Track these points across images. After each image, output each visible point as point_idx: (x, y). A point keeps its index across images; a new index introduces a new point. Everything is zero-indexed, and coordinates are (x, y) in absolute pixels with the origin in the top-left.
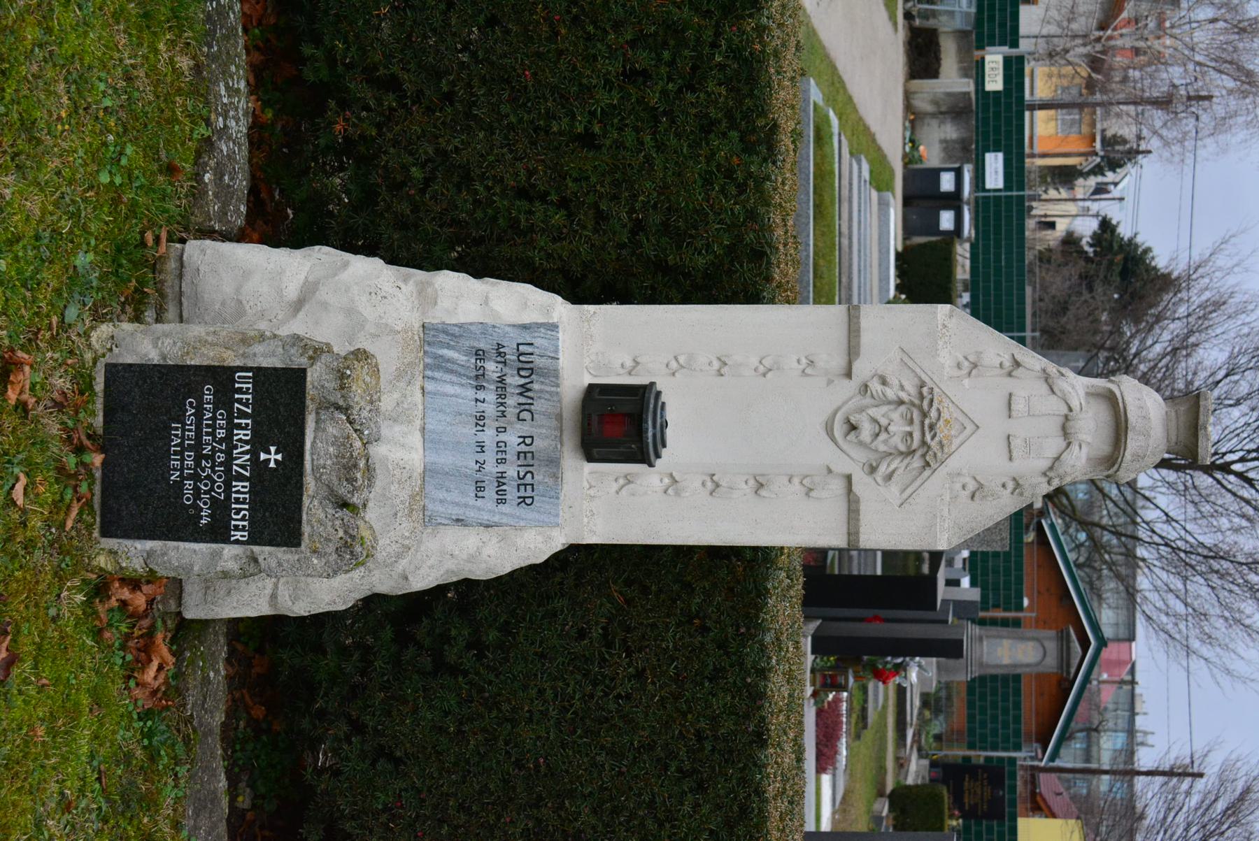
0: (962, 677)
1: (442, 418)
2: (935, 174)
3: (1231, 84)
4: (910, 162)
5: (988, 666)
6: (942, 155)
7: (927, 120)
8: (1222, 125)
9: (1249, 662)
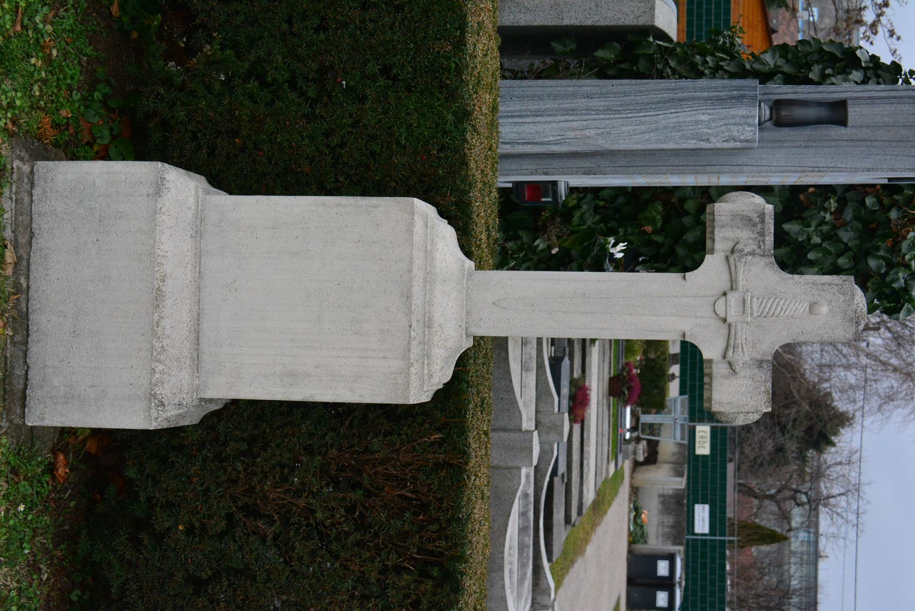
1: (229, 296)
6: (660, 507)
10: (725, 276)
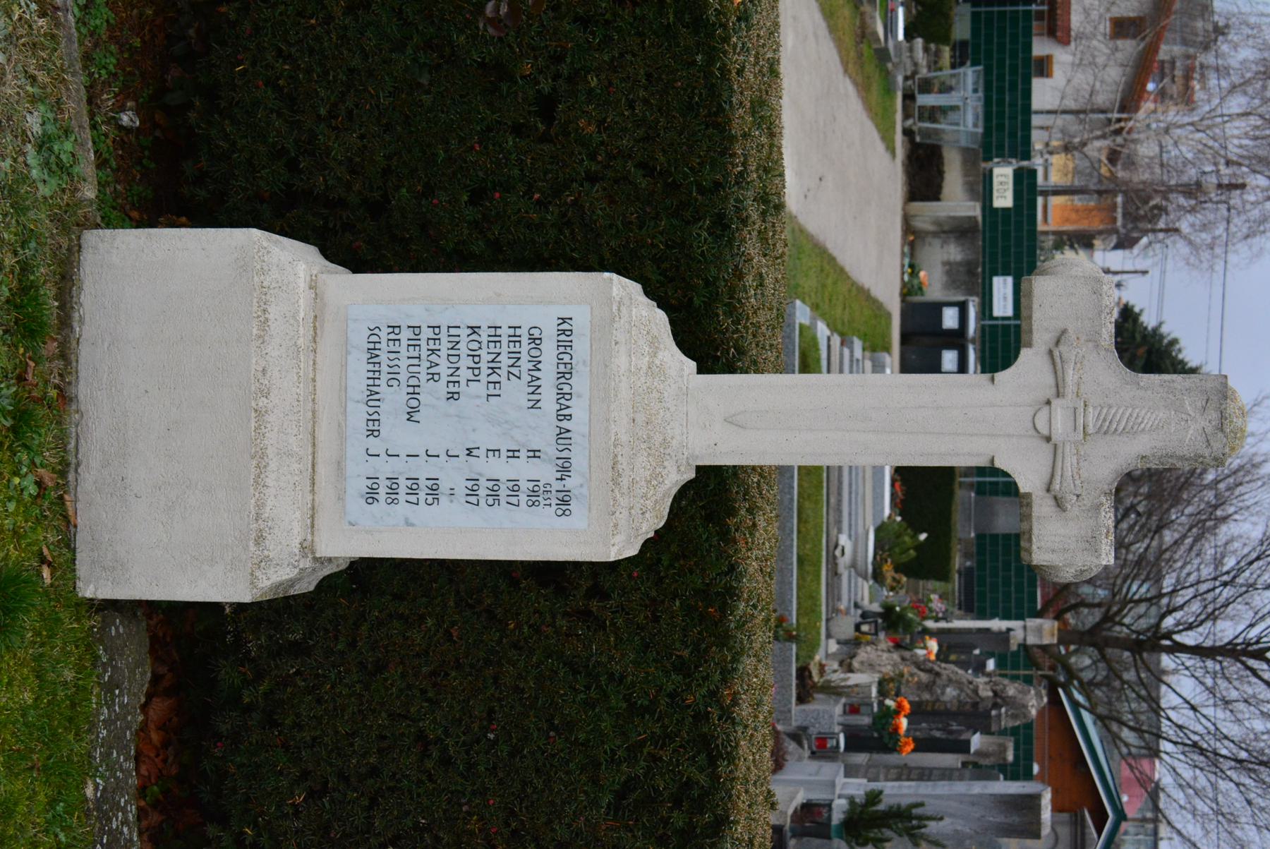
6: (945, 279)
7: (929, 239)
10: (1050, 380)
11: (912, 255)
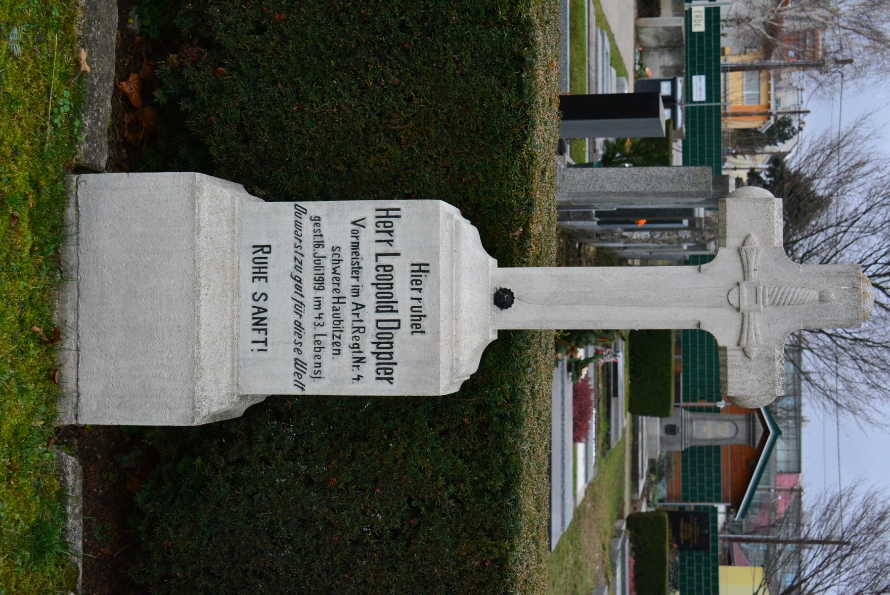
0: (678, 448)
2: (657, 83)
3: (866, 42)
4: (639, 76)
5: (696, 440)
8: (859, 73)
9: (884, 415)
11: (641, 57)
